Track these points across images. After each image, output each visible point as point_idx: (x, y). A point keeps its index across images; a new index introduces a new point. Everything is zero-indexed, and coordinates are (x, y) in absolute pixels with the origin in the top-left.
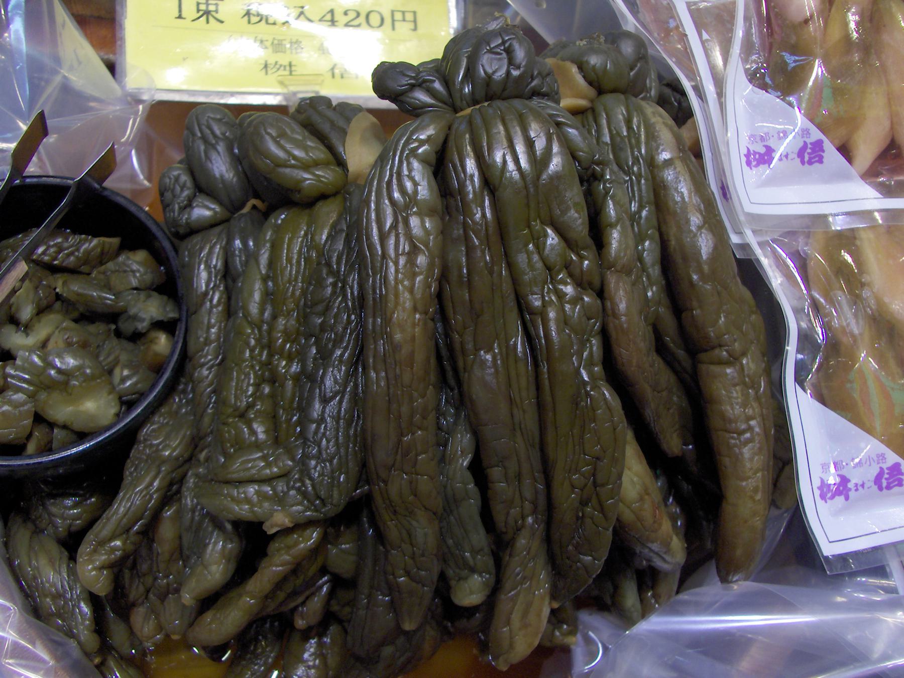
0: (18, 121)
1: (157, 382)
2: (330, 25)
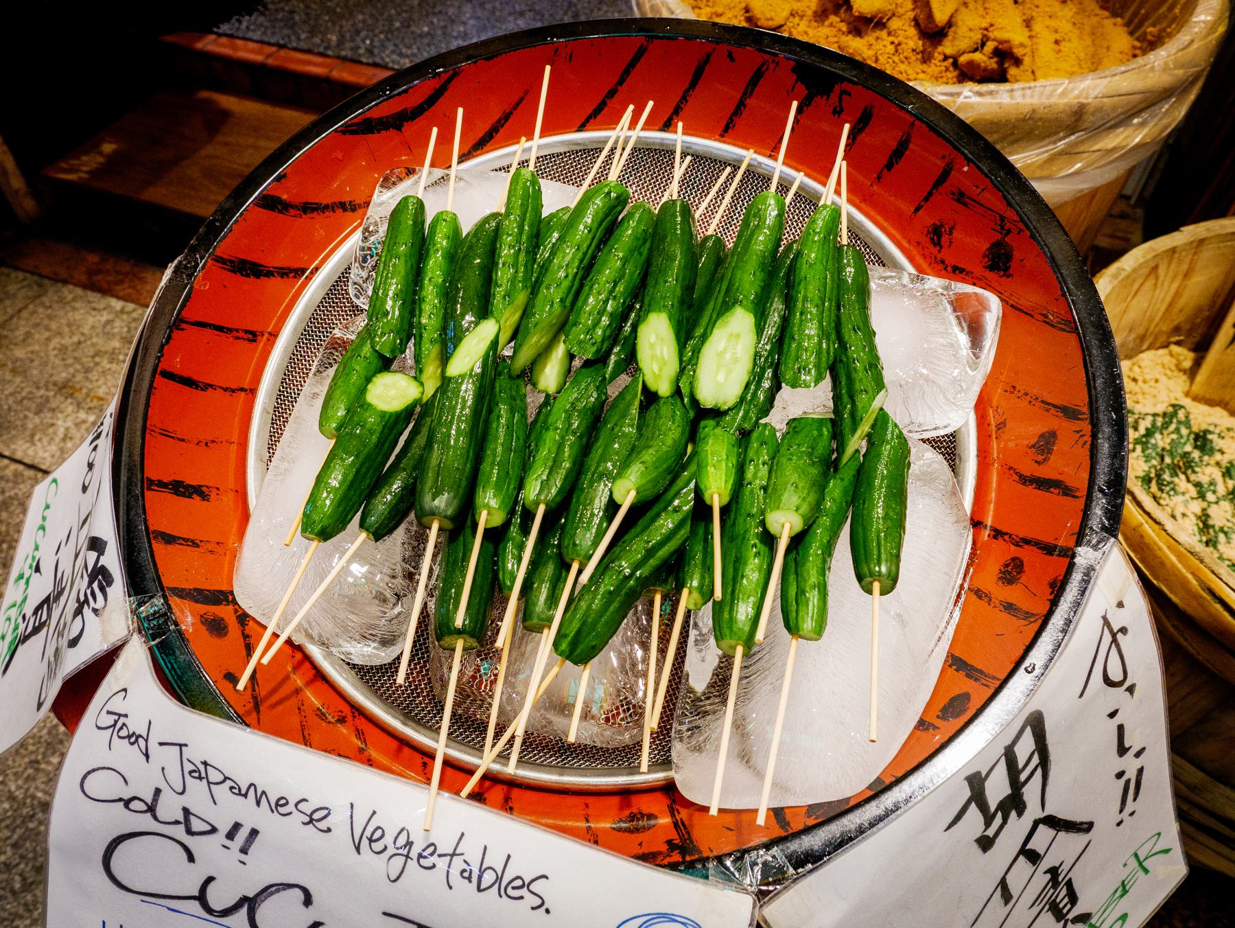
0: (170, 38)
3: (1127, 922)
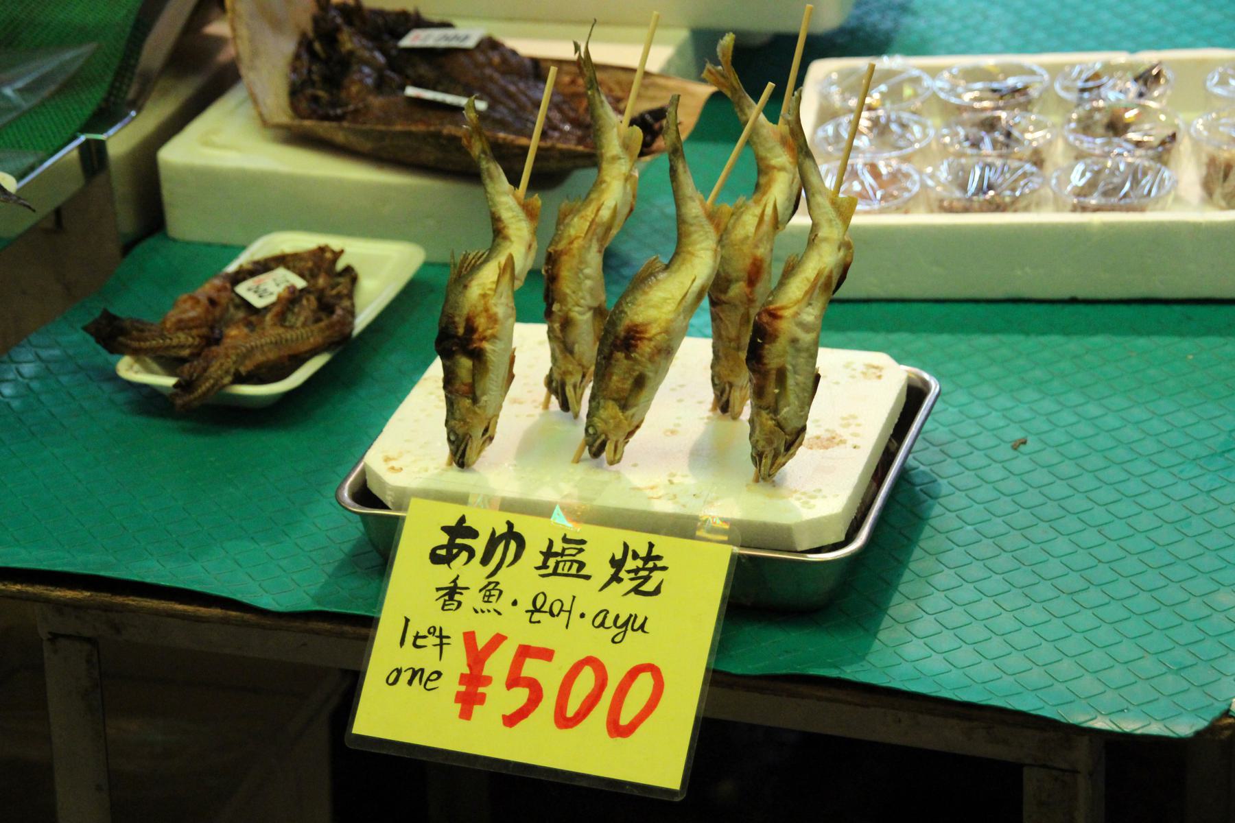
1: (536, 20)
2: (613, 556)
3: (685, 156)
